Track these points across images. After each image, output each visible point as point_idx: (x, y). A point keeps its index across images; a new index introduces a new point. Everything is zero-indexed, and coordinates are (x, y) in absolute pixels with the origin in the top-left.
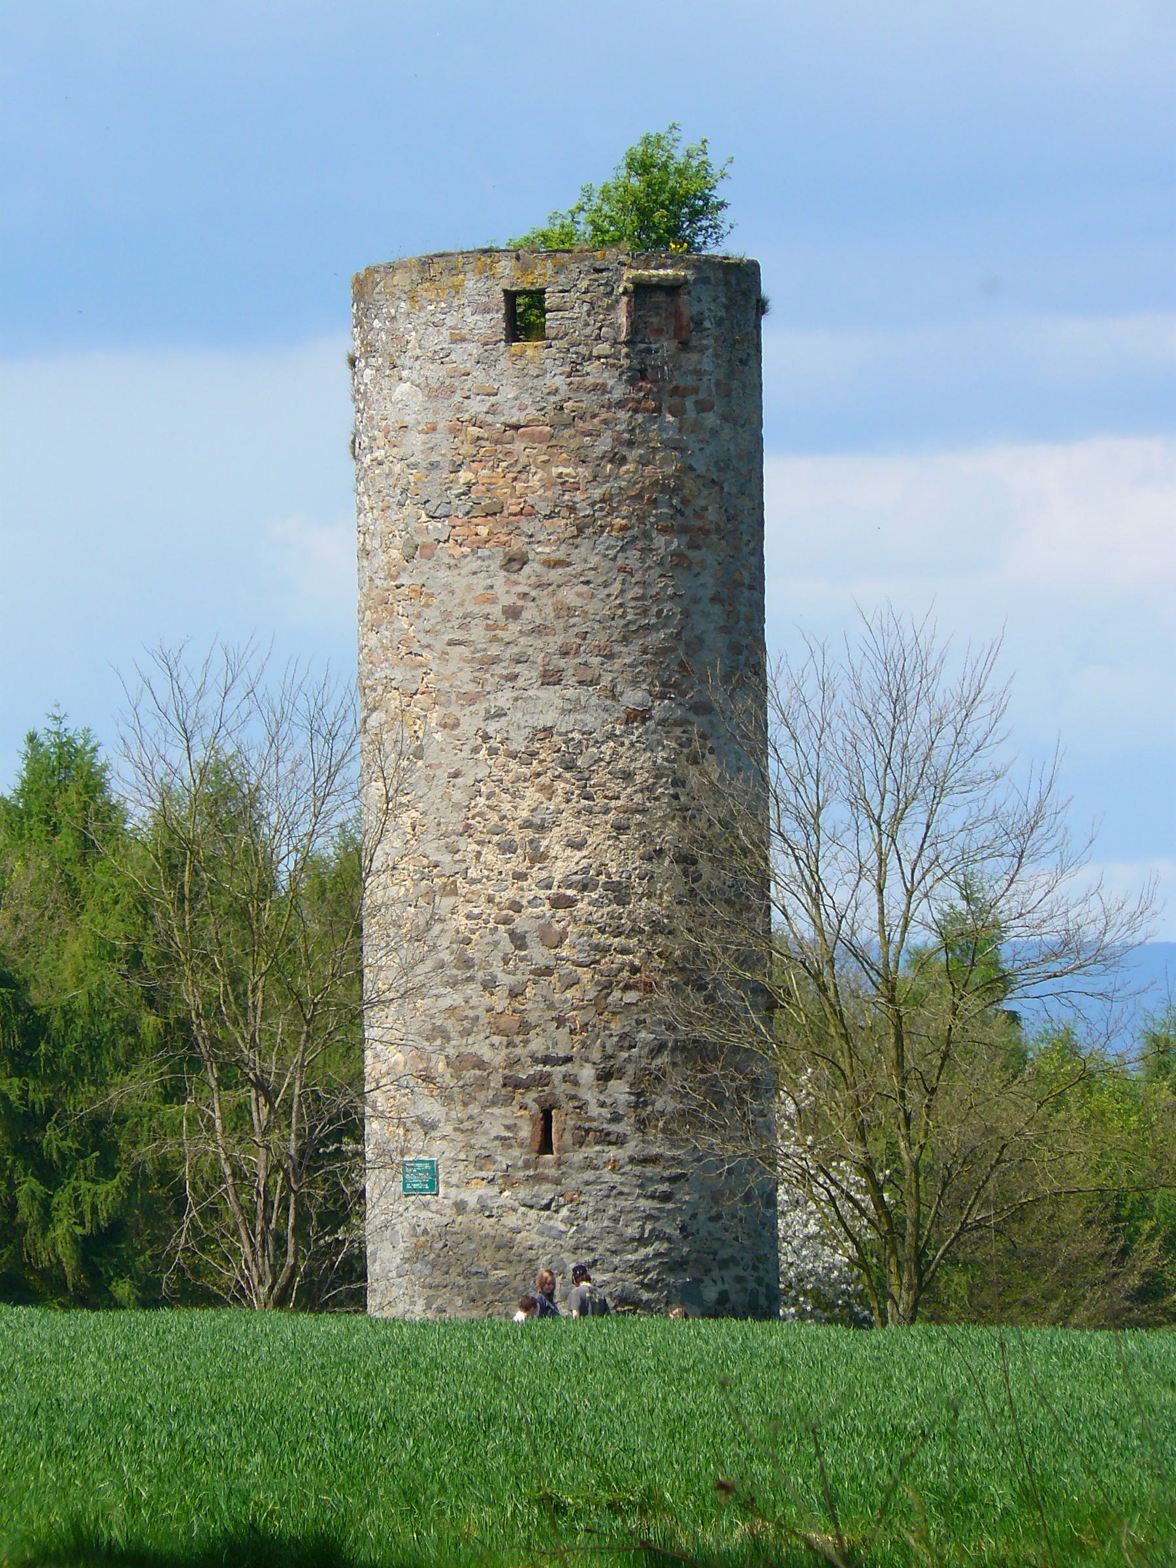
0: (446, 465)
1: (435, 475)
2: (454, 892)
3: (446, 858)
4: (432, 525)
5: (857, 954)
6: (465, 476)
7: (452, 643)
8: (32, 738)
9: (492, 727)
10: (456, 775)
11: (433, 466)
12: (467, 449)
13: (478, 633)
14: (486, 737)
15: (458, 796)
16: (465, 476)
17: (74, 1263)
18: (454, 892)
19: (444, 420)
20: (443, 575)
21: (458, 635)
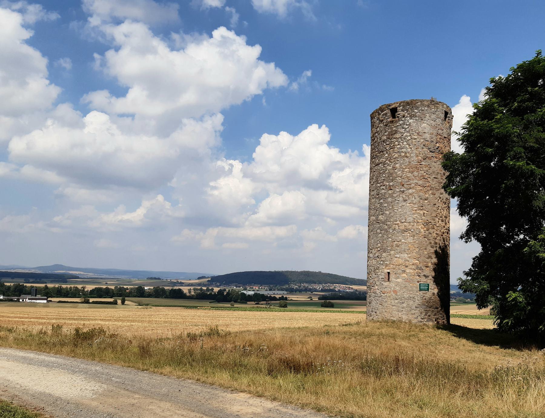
0: (435, 142)
1: (432, 143)
2: (434, 228)
3: (433, 221)
4: (431, 153)
5: (93, 400)
6: (438, 145)
7: (434, 178)
8: (466, 242)
9: (441, 196)
10: (435, 205)
11: (432, 141)
12: (438, 140)
13: (439, 176)
14: (440, 198)
15: (435, 209)
16: (438, 145)
17: (93, 383)
18: (434, 228)
19: (435, 132)
20: (433, 163)
21: (436, 177)
